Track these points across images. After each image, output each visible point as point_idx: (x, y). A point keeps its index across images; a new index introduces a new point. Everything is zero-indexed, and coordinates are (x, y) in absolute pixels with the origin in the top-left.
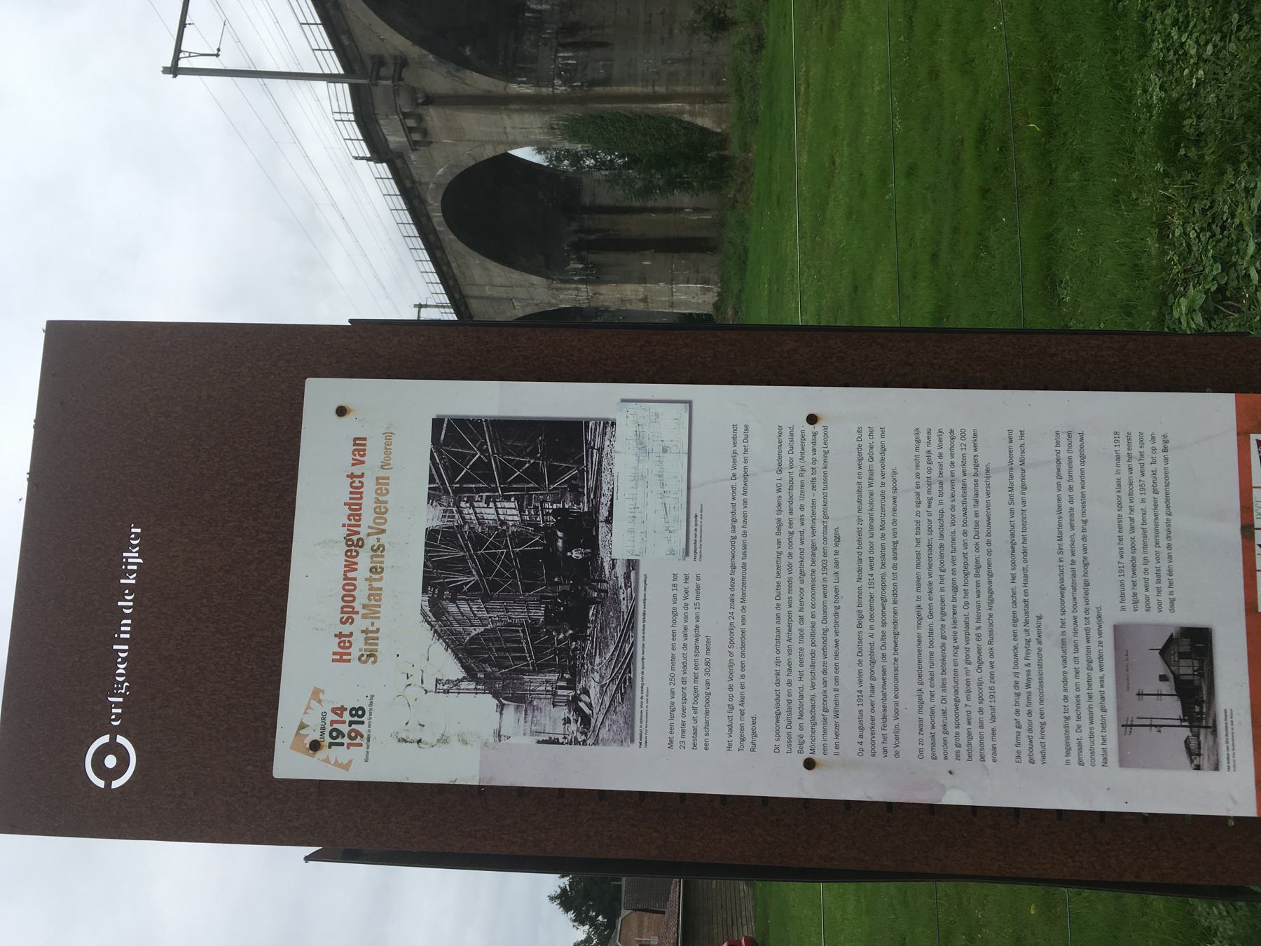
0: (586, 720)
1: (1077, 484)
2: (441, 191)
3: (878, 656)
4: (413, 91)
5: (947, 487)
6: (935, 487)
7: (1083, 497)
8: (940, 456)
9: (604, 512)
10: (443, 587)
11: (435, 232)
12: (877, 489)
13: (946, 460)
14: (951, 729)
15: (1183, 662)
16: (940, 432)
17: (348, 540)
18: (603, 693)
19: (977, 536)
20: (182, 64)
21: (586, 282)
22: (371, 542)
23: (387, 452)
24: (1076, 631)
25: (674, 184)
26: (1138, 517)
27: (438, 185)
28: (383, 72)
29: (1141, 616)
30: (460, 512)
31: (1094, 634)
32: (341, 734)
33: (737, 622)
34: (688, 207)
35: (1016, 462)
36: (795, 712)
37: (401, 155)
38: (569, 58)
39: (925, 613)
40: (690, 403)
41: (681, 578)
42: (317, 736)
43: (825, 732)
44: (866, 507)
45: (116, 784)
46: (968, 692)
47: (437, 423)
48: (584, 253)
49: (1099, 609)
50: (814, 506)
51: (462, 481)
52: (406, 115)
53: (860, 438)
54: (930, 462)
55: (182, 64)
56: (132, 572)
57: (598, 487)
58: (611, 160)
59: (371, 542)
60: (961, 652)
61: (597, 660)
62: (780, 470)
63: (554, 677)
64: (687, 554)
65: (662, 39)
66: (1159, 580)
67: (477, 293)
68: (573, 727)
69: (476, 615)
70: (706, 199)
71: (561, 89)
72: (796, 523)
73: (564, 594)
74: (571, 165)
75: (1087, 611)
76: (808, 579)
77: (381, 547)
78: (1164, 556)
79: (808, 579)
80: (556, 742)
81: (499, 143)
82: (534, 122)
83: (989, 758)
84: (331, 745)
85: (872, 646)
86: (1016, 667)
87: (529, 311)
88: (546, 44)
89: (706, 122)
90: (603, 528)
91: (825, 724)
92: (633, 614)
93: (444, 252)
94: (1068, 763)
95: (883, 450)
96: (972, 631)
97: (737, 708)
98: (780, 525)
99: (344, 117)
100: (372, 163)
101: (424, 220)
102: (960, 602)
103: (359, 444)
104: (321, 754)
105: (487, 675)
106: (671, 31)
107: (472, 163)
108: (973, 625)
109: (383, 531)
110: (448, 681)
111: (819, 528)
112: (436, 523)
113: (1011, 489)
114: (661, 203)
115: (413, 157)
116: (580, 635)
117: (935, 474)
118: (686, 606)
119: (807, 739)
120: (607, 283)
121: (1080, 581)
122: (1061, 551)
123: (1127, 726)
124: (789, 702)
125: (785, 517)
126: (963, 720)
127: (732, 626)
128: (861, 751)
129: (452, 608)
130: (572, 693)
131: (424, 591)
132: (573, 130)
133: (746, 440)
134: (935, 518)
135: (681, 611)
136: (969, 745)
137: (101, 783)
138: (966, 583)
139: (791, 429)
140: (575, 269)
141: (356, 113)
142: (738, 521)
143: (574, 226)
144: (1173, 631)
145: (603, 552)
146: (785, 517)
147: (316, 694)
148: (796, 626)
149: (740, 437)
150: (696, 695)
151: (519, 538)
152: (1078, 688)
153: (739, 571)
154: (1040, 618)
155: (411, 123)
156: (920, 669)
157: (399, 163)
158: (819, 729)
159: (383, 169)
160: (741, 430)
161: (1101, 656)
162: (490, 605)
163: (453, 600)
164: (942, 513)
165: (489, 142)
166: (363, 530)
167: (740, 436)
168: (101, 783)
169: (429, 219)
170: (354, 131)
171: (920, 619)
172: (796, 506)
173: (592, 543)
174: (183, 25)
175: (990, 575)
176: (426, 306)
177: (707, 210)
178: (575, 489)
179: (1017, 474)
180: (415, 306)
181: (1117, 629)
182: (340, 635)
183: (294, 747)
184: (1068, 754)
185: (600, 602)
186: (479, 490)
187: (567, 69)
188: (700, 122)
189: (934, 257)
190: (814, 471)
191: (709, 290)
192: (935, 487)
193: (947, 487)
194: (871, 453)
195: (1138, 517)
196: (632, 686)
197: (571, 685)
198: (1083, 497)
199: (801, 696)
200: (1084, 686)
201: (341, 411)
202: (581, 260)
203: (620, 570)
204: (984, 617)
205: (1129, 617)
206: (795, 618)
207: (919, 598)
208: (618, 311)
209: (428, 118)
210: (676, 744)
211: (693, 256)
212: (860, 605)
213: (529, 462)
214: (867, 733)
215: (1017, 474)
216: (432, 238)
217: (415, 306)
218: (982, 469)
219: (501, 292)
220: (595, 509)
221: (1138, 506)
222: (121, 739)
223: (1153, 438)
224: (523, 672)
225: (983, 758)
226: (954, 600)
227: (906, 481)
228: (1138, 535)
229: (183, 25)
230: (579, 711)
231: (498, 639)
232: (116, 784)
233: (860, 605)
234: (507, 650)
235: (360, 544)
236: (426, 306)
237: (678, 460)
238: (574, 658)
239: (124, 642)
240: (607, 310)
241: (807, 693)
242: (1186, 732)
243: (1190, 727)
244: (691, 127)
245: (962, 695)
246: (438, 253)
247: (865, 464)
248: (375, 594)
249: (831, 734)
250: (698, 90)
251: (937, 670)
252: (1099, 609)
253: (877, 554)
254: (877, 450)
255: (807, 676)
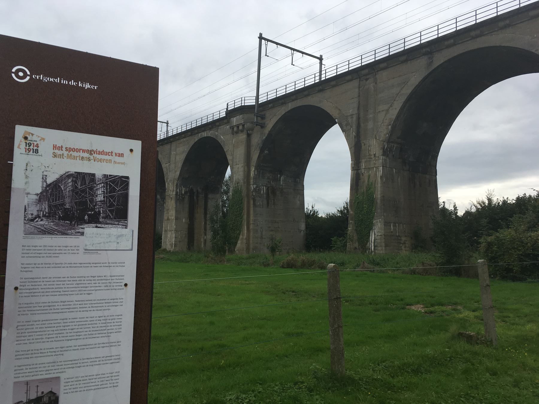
0: (32, 220)
1: (105, 362)
2: (214, 137)
3: (51, 308)
4: (252, 129)
5: (104, 325)
6: (104, 322)
7: (100, 364)
8: (114, 322)
9: (99, 225)
10: (77, 178)
11: (198, 133)
12: (104, 305)
13: (112, 324)
14: (27, 331)
15: (48, 398)
16: (121, 322)
17: (92, 150)
18: (41, 225)
19: (89, 335)
20: (263, 41)
21: (176, 194)
22: (92, 157)
23: (119, 163)
24: (58, 366)
25: (215, 233)
26: (93, 381)
27: (217, 136)
28: (259, 118)
29: (62, 384)
30: (100, 184)
31: (57, 371)
32: (30, 146)
33: (63, 265)
34: (206, 238)
35: (111, 344)
36: (34, 284)
37: (228, 122)
38: (263, 191)
39: (65, 321)
40: (132, 250)
41: (78, 248)
42: (29, 139)
43: (27, 293)
44: (99, 302)
45: (13, 75)
46: (39, 335)
47: (128, 178)
48: (188, 194)
49: (65, 372)
50: (100, 286)
51: (110, 186)
52: (243, 126)
53: (120, 299)
54: (112, 319)
55: (263, 41)
56: (83, 85)
57: (107, 224)
58: (225, 206)
59: (92, 157)
60: (52, 332)
61: (52, 224)
62: (111, 276)
63: (47, 211)
64: (86, 250)
65: (270, 227)
66: (73, 389)
67: (172, 148)
68: (30, 216)
69: (68, 187)
70: (209, 244)
71: (252, 187)
72: (94, 282)
73: (74, 214)
74: (224, 190)
75: (64, 368)
76: (77, 286)
77: (90, 160)
78: (81, 389)
79: (77, 286)
80: (25, 211)
81: (233, 161)
82: (240, 176)
83: (17, 343)
84: (26, 143)
85: (55, 306)
86: (47, 349)
87: (164, 170)
88: (268, 182)
89: (239, 245)
90: (94, 225)
91: (29, 293)
92: (67, 234)
93: (190, 136)
94: (15, 366)
95: (116, 306)
96: (59, 335)
97: (35, 266)
98: (94, 277)
99: (243, 102)
100: (225, 110)
101: (203, 129)
102: (68, 331)
103: (121, 155)
104: (23, 140)
105: (48, 190)
106: (272, 231)
107: (225, 150)
108: (61, 335)
109: (95, 161)
110: (46, 179)
111: (93, 288)
112: (97, 176)
113: (103, 343)
114: (208, 227)
115: (228, 127)
116: (60, 218)
117: (108, 321)
118: (69, 250)
119: (24, 288)
120: (176, 203)
121: (74, 366)
122: (83, 359)
123: (27, 383)
124: (37, 282)
125: (96, 278)
126: (30, 334)
127: (62, 264)
128: (20, 304)
129: (70, 180)
130: (41, 216)
131: (76, 172)
132: (237, 191)
133: (120, 266)
134: (95, 322)
135: (67, 248)
136: (22, 336)
137: (14, 70)
138: (74, 332)
139: (123, 279)
140: (182, 190)
141: (244, 106)
142: (96, 265)
143: (200, 190)
144: (58, 394)
145: (86, 225)
146: (96, 278)
147: (43, 139)
148: (62, 283)
149: (121, 265)
150: (39, 254)
151: (92, 201)
152: (40, 368)
153: (80, 265)
154: (63, 355)
155: (241, 127)
156: (47, 320)
157: (225, 121)
158: (28, 291)
159: (223, 114)
160: (123, 265)
161: (50, 374)
162: (71, 192)
163: (72, 181)
164: (96, 324)
165: (233, 158)
166: (95, 155)
167: (122, 264)
168: (14, 70)
169: (204, 131)
170: (238, 105)
171: (63, 320)
172: (99, 281)
173: (89, 222)
174: (277, 44)
175: (77, 339)
176: (167, 126)
177: (205, 245)
178: (105, 217)
179: (108, 345)
180: (168, 121)
181: (59, 378)
182: (62, 147)
183: (26, 132)
184: (18, 366)
185: (71, 224)
186: (107, 189)
187: (260, 190)
188: (239, 242)
189: (180, 334)
190: (110, 286)
191: (172, 247)
192: (104, 322)
193: (104, 325)
194: (115, 302)
195: (93, 381)
196: (43, 234)
197: (44, 216)
198: (100, 364)
199: (39, 285)
200: (40, 369)
201: (131, 150)
202: (186, 193)
203: (81, 230)
204: (63, 339)
205: (62, 381)
206: (64, 283)
207: (70, 319)
208: (164, 208)
209: (242, 134)
210: (24, 248)
211: (186, 240)
212: (68, 302)
213: (115, 204)
214: (26, 305)
215: (108, 345)
216: (196, 131)
217: (168, 121)
218: (109, 335)
219: (172, 158)
220: (100, 223)
221: (97, 380)
222: (28, 78)
223: (117, 383)
224: (49, 201)
225: (17, 341)
226: (69, 329)
227: (106, 313)
228: (89, 381)
229: (277, 44)
230: (36, 218)
231: (59, 194)
232: (13, 75)
233: (68, 302)
234: (56, 197)
235: (91, 154)
236: (167, 126)
237: (115, 247)
238: (53, 217)
239: (60, 81)
240: (164, 203)
241: (40, 287)
242: (25, 401)
243: (27, 402)
244: (237, 238)
245: (38, 333)
246: (190, 133)
247: (112, 301)
248: (75, 158)
249: (26, 295)
250: (251, 242)
251: (46, 326)
252: (65, 372)
253: (84, 306)
254: (116, 304)
255: (45, 287)
